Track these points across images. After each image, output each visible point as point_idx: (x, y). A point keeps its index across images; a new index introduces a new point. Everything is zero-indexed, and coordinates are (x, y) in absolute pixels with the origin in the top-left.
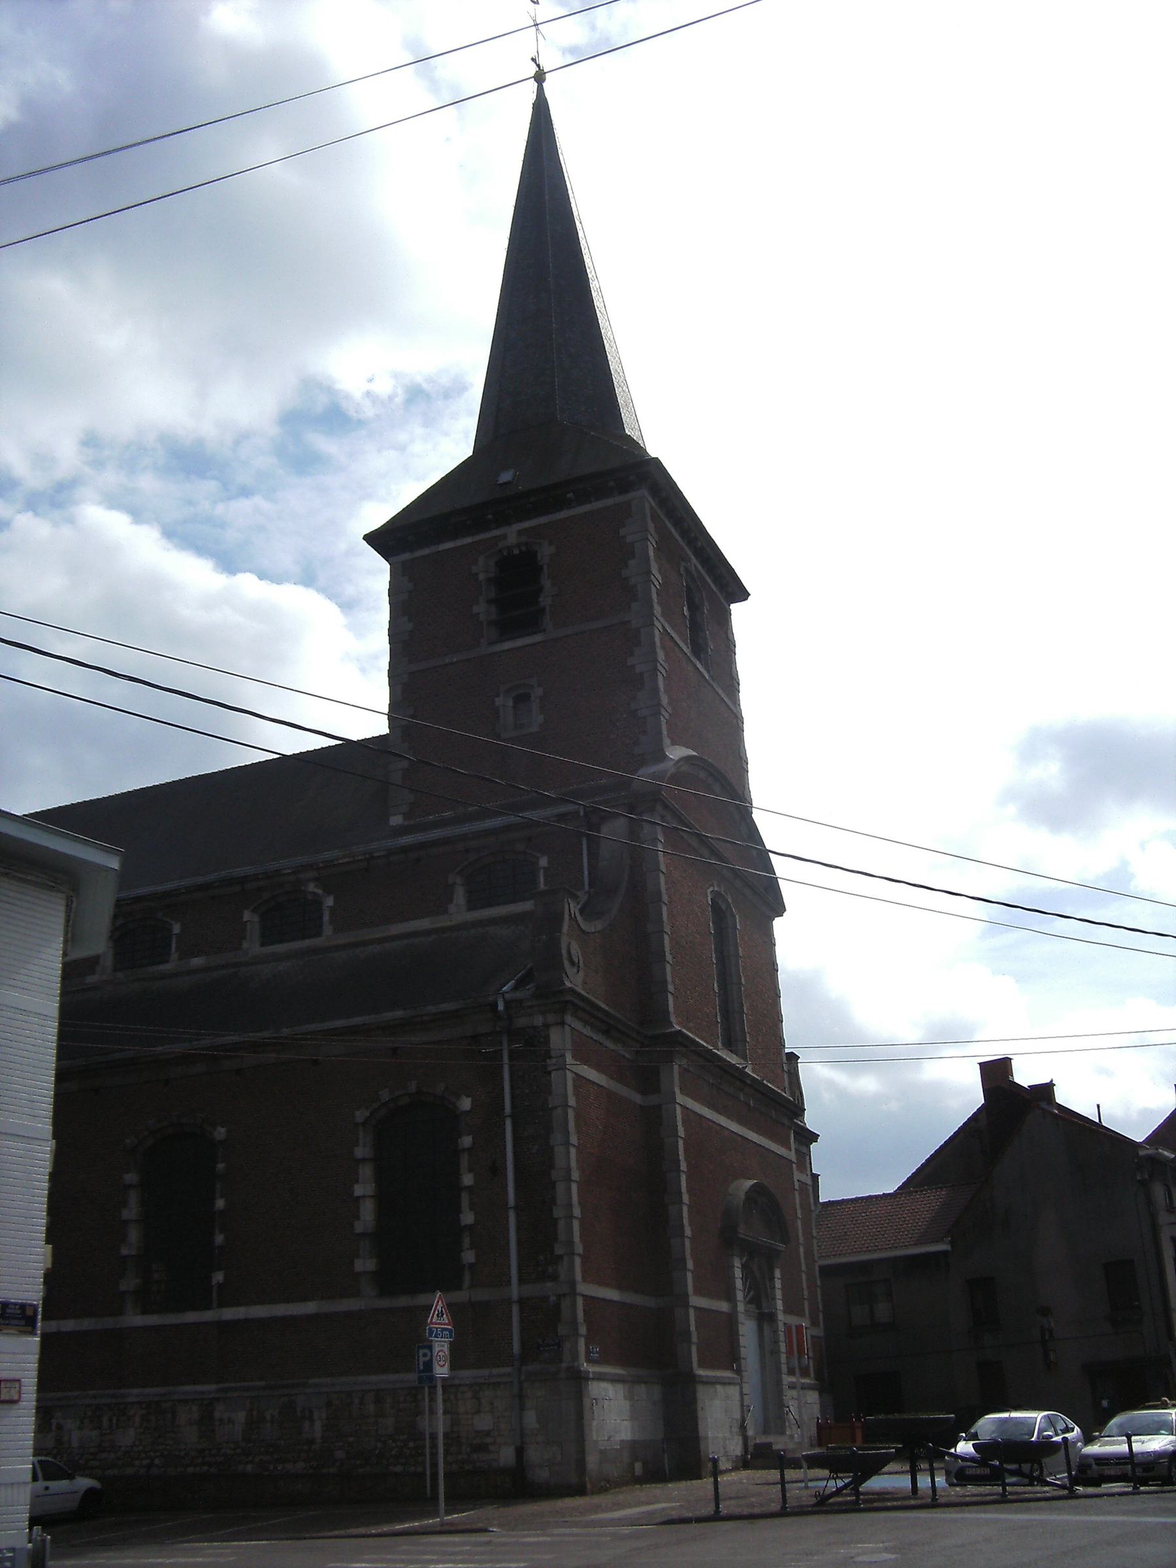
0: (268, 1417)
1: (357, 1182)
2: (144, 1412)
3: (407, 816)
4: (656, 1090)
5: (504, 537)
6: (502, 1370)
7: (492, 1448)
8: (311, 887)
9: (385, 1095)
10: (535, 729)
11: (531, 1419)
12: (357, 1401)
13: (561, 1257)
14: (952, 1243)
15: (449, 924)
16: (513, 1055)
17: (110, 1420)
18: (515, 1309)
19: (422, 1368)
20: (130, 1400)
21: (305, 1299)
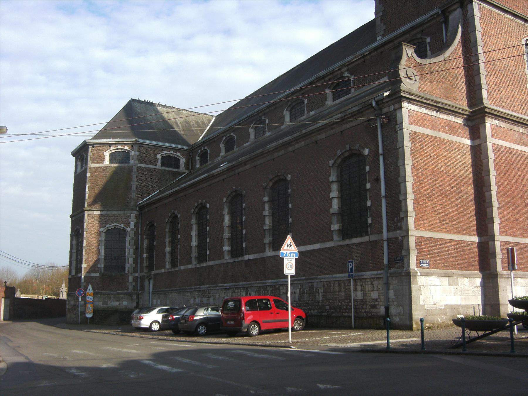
0: (306, 291)
1: (331, 192)
2: (271, 289)
4: (479, 137)
6: (379, 272)
7: (377, 306)
8: (346, 74)
9: (339, 153)
11: (391, 294)
12: (332, 285)
13: (403, 218)
16: (382, 126)
17: (263, 292)
18: (385, 245)
19: (349, 271)
20: (267, 284)
21: (315, 243)
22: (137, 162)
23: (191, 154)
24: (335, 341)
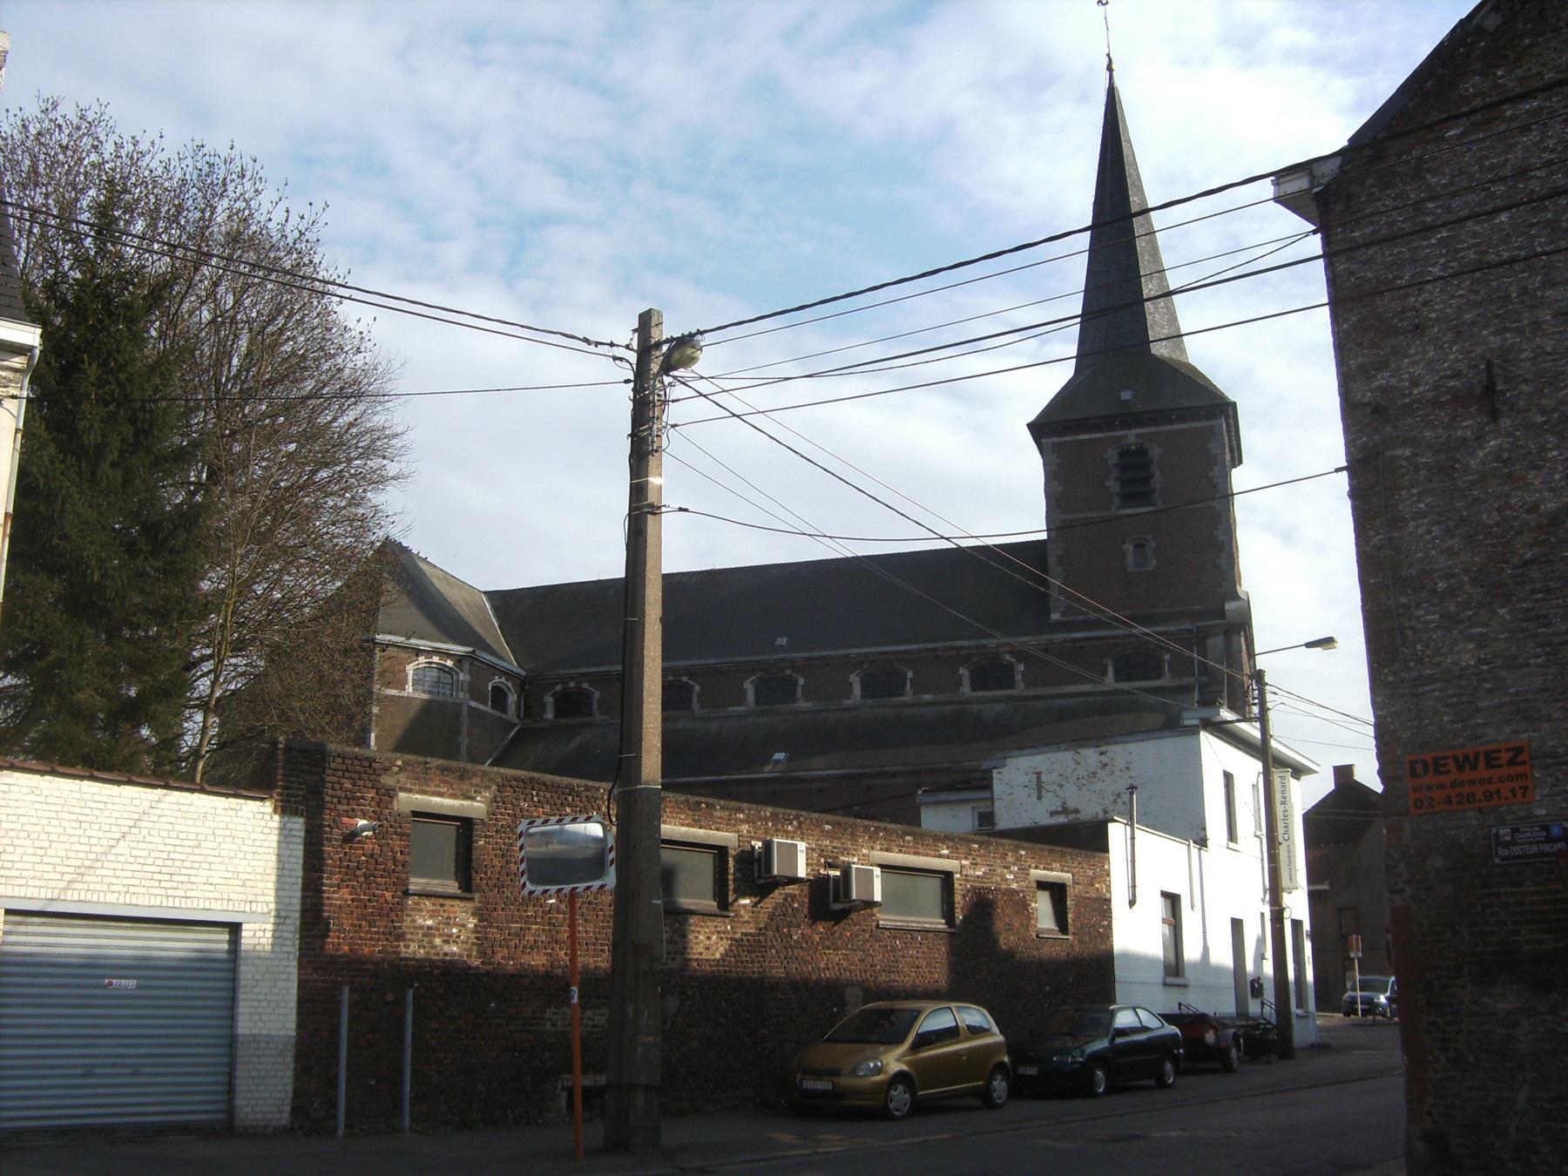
3: (1062, 614)
5: (1126, 437)
8: (1008, 657)
10: (1150, 568)
14: (1330, 885)
15: (1102, 689)
22: (468, 696)
23: (527, 687)
24: (929, 923)
